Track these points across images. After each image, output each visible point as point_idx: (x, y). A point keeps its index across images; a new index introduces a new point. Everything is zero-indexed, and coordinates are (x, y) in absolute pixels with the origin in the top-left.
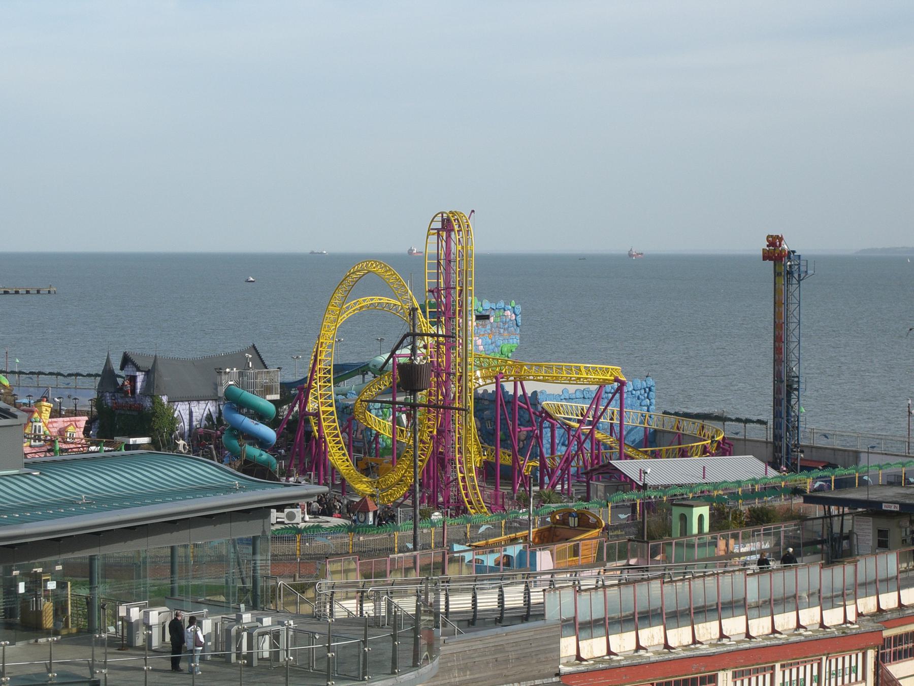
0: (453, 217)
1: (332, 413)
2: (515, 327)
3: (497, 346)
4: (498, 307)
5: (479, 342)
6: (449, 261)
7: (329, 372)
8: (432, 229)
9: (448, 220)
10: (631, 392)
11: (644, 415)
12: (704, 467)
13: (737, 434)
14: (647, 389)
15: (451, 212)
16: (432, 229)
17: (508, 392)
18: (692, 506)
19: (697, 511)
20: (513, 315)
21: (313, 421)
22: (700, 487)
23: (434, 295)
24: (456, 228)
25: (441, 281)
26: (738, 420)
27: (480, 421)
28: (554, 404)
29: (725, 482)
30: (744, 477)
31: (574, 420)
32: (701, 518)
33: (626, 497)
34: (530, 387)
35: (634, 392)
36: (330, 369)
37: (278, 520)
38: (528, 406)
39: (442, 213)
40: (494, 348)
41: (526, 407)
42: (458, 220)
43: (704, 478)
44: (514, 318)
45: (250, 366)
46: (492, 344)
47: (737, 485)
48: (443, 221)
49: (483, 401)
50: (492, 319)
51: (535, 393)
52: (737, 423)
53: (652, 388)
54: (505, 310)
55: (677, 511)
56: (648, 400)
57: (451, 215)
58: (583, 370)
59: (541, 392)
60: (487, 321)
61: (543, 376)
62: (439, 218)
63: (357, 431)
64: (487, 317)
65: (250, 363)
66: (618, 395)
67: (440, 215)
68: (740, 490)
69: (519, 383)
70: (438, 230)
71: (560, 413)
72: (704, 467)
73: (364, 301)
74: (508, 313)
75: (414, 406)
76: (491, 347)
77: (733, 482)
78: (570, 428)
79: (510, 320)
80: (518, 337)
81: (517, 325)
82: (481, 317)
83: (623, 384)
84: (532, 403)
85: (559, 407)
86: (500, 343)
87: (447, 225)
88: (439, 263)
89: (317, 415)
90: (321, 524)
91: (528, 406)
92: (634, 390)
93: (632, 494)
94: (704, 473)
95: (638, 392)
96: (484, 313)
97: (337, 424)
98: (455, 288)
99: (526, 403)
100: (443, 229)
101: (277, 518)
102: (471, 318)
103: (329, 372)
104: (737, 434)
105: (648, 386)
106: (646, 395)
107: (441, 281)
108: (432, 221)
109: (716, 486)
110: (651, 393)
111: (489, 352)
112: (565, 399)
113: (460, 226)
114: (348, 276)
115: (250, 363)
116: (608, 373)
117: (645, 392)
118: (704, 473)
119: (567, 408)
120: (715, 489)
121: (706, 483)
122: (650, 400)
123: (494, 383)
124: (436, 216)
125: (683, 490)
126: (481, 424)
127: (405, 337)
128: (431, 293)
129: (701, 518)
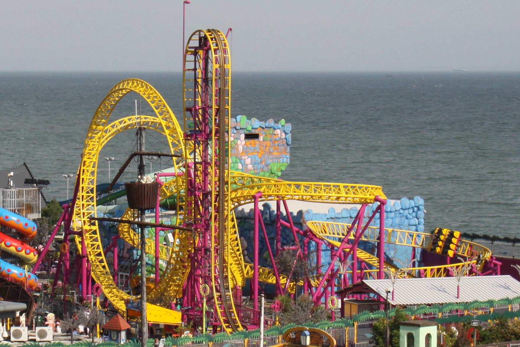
0: (210, 35)
1: (95, 232)
2: (286, 145)
3: (267, 165)
4: (267, 126)
5: (248, 161)
6: (206, 80)
7: (92, 191)
8: (190, 48)
9: (205, 38)
10: (399, 210)
11: (412, 234)
12: (458, 287)
13: (505, 253)
14: (416, 209)
15: (209, 31)
16: (190, 48)
17: (292, 213)
18: (419, 326)
19: (423, 331)
20: (283, 134)
21: (78, 239)
22: (450, 307)
23: (191, 113)
24: (213, 47)
25: (199, 99)
26: (507, 240)
27: (246, 240)
28: (319, 223)
29: (476, 302)
30: (483, 298)
31: (334, 239)
32: (428, 336)
33: (372, 316)
34: (294, 207)
35: (402, 211)
36: (93, 188)
37: (30, 338)
38: (290, 224)
39: (200, 31)
40: (264, 167)
41: (288, 225)
42: (215, 39)
43: (458, 298)
44: (284, 137)
45: (12, 185)
46: (261, 162)
47: (489, 305)
48: (200, 39)
49: (249, 221)
50: (261, 138)
51: (300, 213)
52: (506, 243)
53: (420, 207)
54: (275, 129)
55: (404, 333)
56: (416, 219)
57: (207, 34)
58: (342, 189)
59: (307, 212)
60: (256, 141)
61: (291, 195)
62: (196, 37)
63: (123, 250)
64: (256, 136)
65: (12, 182)
66: (378, 215)
67: (198, 33)
68: (492, 310)
69: (282, 202)
70: (196, 48)
71: (325, 232)
72: (458, 287)
73: (129, 120)
74: (278, 132)
75: (143, 226)
76: (260, 166)
77: (484, 302)
78: (333, 247)
79: (280, 138)
80: (288, 156)
81: (288, 145)
82: (251, 136)
83: (383, 203)
84: (295, 221)
85: (324, 226)
86: (269, 161)
87: (204, 42)
88: (196, 82)
89: (80, 234)
90: (62, 342)
91: (290, 224)
92: (402, 209)
93: (379, 313)
94: (458, 292)
95: (407, 211)
96: (254, 132)
97: (99, 243)
98: (211, 107)
99: (288, 222)
100: (200, 47)
101: (28, 336)
102: (288, 136)
103: (92, 191)
104: (505, 253)
105: (417, 205)
106: (414, 214)
107: (199, 99)
108: (190, 39)
109: (466, 305)
110: (419, 212)
111: (258, 171)
112: (331, 218)
113: (217, 45)
114: (110, 94)
115: (12, 182)
116: (368, 192)
117: (414, 211)
118: (458, 292)
119: (333, 227)
120: (465, 309)
121: (457, 303)
122: (418, 219)
123: (252, 202)
124: (194, 34)
125: (432, 310)
126: (248, 243)
127: (132, 157)
128: (189, 112)
129: (428, 336)
